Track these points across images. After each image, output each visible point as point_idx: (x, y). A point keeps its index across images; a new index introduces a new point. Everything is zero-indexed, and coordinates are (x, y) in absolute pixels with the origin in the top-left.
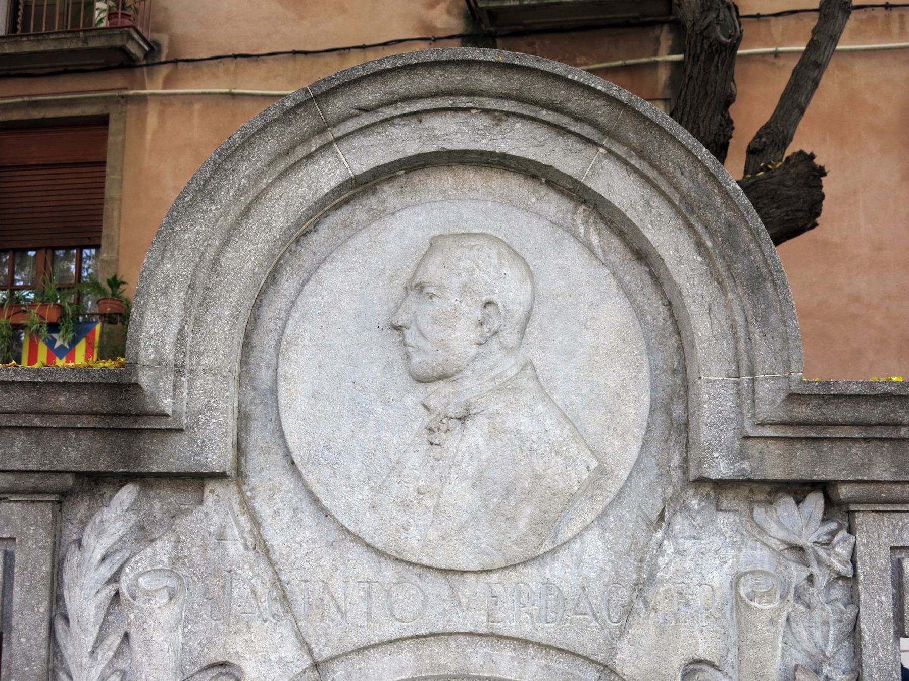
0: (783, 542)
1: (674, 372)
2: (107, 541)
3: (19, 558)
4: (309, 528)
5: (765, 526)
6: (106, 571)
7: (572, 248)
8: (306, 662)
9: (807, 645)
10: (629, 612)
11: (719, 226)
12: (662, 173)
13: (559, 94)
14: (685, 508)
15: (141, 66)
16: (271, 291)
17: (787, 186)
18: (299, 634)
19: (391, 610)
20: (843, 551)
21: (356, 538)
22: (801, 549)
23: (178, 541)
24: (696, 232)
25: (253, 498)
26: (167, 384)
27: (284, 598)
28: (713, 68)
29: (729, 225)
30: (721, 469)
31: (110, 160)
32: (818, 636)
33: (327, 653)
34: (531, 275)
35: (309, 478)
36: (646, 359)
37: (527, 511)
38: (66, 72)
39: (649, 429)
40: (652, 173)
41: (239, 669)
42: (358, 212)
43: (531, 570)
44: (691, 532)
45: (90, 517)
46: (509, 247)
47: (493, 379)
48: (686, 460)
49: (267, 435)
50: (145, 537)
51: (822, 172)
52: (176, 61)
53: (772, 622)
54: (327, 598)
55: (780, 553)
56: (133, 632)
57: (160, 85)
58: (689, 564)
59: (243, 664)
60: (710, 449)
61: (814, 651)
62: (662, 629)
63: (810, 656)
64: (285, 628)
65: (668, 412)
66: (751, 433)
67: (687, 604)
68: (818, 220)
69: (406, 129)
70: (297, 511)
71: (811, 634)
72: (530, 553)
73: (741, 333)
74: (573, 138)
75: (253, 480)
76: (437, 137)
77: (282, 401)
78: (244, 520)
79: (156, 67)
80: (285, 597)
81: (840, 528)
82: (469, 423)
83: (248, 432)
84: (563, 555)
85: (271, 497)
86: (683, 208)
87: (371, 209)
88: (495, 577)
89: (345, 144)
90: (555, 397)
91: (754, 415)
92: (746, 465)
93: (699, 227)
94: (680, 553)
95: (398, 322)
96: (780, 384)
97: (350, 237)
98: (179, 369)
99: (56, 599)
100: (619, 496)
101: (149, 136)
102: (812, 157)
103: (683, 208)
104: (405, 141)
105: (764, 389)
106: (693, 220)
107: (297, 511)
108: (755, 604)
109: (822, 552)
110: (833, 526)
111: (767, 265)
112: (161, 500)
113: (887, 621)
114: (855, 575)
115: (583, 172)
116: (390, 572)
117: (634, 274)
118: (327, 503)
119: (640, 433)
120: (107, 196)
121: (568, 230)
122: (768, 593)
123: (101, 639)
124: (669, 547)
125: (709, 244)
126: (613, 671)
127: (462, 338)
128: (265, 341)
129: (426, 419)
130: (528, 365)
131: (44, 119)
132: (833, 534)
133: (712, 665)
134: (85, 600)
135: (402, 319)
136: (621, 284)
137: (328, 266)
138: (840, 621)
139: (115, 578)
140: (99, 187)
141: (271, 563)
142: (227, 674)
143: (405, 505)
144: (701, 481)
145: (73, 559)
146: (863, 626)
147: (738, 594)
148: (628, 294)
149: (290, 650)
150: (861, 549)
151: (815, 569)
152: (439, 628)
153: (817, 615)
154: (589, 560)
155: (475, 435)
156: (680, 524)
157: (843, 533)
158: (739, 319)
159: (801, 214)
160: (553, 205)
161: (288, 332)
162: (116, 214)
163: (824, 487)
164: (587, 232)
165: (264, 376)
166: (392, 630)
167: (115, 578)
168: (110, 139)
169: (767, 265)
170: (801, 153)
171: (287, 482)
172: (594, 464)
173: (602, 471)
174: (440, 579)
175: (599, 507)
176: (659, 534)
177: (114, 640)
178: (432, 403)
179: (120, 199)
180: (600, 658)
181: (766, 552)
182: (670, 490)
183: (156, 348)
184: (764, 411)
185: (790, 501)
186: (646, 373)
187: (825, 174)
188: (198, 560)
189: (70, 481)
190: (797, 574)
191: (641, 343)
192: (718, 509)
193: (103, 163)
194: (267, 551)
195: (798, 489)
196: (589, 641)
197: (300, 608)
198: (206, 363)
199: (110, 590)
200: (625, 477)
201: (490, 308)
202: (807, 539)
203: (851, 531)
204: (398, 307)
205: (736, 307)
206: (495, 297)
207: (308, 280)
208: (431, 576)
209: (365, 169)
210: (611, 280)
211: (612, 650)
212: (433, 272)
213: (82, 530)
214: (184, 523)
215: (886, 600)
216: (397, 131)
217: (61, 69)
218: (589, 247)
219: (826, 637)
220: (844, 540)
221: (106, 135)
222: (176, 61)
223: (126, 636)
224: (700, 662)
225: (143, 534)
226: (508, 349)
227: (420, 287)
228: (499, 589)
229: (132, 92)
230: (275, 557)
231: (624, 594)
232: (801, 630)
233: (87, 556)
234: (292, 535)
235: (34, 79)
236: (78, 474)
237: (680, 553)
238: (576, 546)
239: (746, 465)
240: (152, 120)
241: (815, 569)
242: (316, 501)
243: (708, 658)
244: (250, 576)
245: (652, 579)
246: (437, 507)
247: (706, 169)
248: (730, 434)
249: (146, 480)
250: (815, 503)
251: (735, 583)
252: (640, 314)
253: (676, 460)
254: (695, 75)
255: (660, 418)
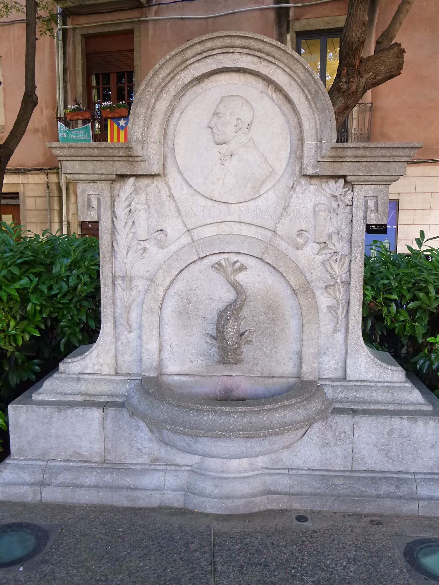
0: (331, 194)
1: (299, 140)
2: (127, 194)
3: (102, 199)
4: (186, 189)
5: (325, 189)
6: (127, 203)
7: (266, 99)
8: (186, 230)
9: (336, 226)
10: (282, 216)
11: (313, 91)
12: (295, 73)
13: (261, 46)
14: (300, 183)
15: (145, 7)
16: (172, 116)
17: (389, 58)
18: (183, 222)
19: (210, 214)
20: (349, 197)
21: (200, 194)
22: (335, 196)
23: (147, 194)
24: (305, 93)
25: (168, 181)
26: (140, 147)
27: (179, 211)
28: (359, 10)
29: (316, 91)
30: (310, 171)
31: (136, 49)
32: (339, 223)
33: (192, 227)
34: (253, 109)
35: (185, 175)
36: (289, 136)
37: (249, 184)
38: (116, 11)
39: (289, 159)
40: (292, 73)
41: (166, 232)
42: (198, 88)
43: (251, 203)
44: (302, 191)
45: (121, 187)
46: (246, 100)
47: (240, 144)
48: (301, 169)
49: (172, 162)
50: (138, 194)
51: (404, 51)
52: (159, 4)
53: (325, 219)
54: (191, 211)
55: (329, 198)
56: (135, 221)
57: (153, 15)
58: (300, 201)
59: (167, 230)
60: (307, 165)
61: (337, 227)
62: (291, 221)
63: (337, 229)
64: (179, 220)
65: (296, 153)
66: (320, 160)
67: (299, 213)
68: (402, 71)
69: (212, 60)
70: (181, 185)
71: (337, 222)
72: (251, 198)
73: (318, 127)
74: (267, 62)
75: (169, 176)
76: (222, 63)
77: (176, 151)
78: (166, 188)
79: (151, 7)
80: (179, 211)
81: (349, 190)
82: (233, 157)
83: (166, 161)
84: (261, 198)
85: (174, 181)
86: (301, 85)
87: (202, 88)
88: (241, 204)
89: (193, 66)
90: (260, 149)
91: (321, 154)
92: (318, 170)
93: (306, 92)
94: (298, 198)
95: (210, 126)
96: (329, 144)
97: (196, 97)
98: (143, 142)
99: (113, 212)
100: (280, 179)
101: (150, 38)
102: (400, 45)
103: (301, 85)
104: (211, 64)
105: (324, 146)
106: (304, 89)
107: (181, 185)
108: (320, 213)
109: (342, 198)
110: (347, 189)
111: (327, 104)
112: (142, 182)
113: (361, 219)
114: (352, 205)
115: (269, 73)
116: (210, 203)
117: (286, 107)
118: (190, 183)
119: (286, 160)
120: (135, 64)
121: (266, 93)
122: (324, 210)
123: (126, 223)
124: (295, 196)
125: (309, 97)
126: (276, 233)
127: (230, 130)
128: (170, 132)
129: (220, 156)
130: (252, 138)
131: (109, 32)
132: (346, 192)
133: (306, 231)
134: (121, 211)
135: (212, 124)
136: (282, 112)
137: (189, 107)
138: (346, 219)
139: (130, 205)
140: (132, 60)
141: (175, 201)
142: (163, 233)
143: (213, 183)
144: (305, 176)
145: (117, 200)
146: (354, 220)
147: (315, 211)
148: (285, 115)
149: (181, 226)
150: (355, 196)
151: (340, 203)
152: (224, 220)
153: (339, 217)
154: (269, 199)
155: (234, 161)
156: (298, 189)
157: (350, 191)
158: (318, 123)
159: (393, 70)
160: (261, 84)
161: (177, 130)
162: (139, 72)
163: (344, 177)
164: (272, 94)
165: (170, 143)
166: (210, 221)
167: (130, 205)
168: (135, 39)
169: (327, 104)
170: (396, 43)
171: (178, 177)
172: (271, 170)
173: (273, 172)
174: (224, 205)
175: (273, 183)
176: (291, 192)
177: (130, 223)
178: (221, 152)
179: (141, 66)
180: (272, 229)
181: (325, 197)
182: (295, 178)
183: (137, 136)
184: (324, 153)
185: (333, 181)
186: (289, 141)
187: (405, 52)
188: (153, 200)
189: (114, 176)
190: (334, 204)
191: (288, 131)
192: (311, 184)
193: (133, 50)
194: (173, 197)
195: (336, 177)
196: (270, 224)
197: (183, 214)
198: (152, 140)
199: (128, 209)
200: (281, 174)
201: (239, 121)
202: (337, 194)
203: (352, 191)
204: (211, 121)
205: (317, 118)
206: (240, 117)
207: (182, 112)
208: (222, 204)
209: (199, 74)
210: (279, 110)
211: (276, 227)
212: (221, 108)
213: (119, 191)
214: (149, 189)
215: (362, 213)
216: (209, 61)
217: (114, 9)
218: (272, 99)
219: (342, 224)
220: (350, 194)
221: (133, 38)
222: (159, 4)
223: (134, 222)
224: (302, 230)
225: (136, 190)
226: (246, 134)
227: (217, 114)
228: (242, 209)
229: (142, 19)
230: (176, 199)
231: (280, 210)
232: (334, 221)
233: (121, 199)
234: (181, 191)
235: (103, 15)
236: (117, 175)
237: (298, 198)
238: (266, 195)
239: (318, 170)
240: (151, 31)
241: (340, 203)
242: (187, 182)
243: (305, 229)
244: (169, 205)
245: (289, 205)
246: (223, 184)
247: (309, 72)
248: (313, 160)
249: (137, 176)
250: (341, 181)
251: (314, 207)
252: (288, 122)
253: (298, 169)
254: (352, 13)
255: (293, 155)
